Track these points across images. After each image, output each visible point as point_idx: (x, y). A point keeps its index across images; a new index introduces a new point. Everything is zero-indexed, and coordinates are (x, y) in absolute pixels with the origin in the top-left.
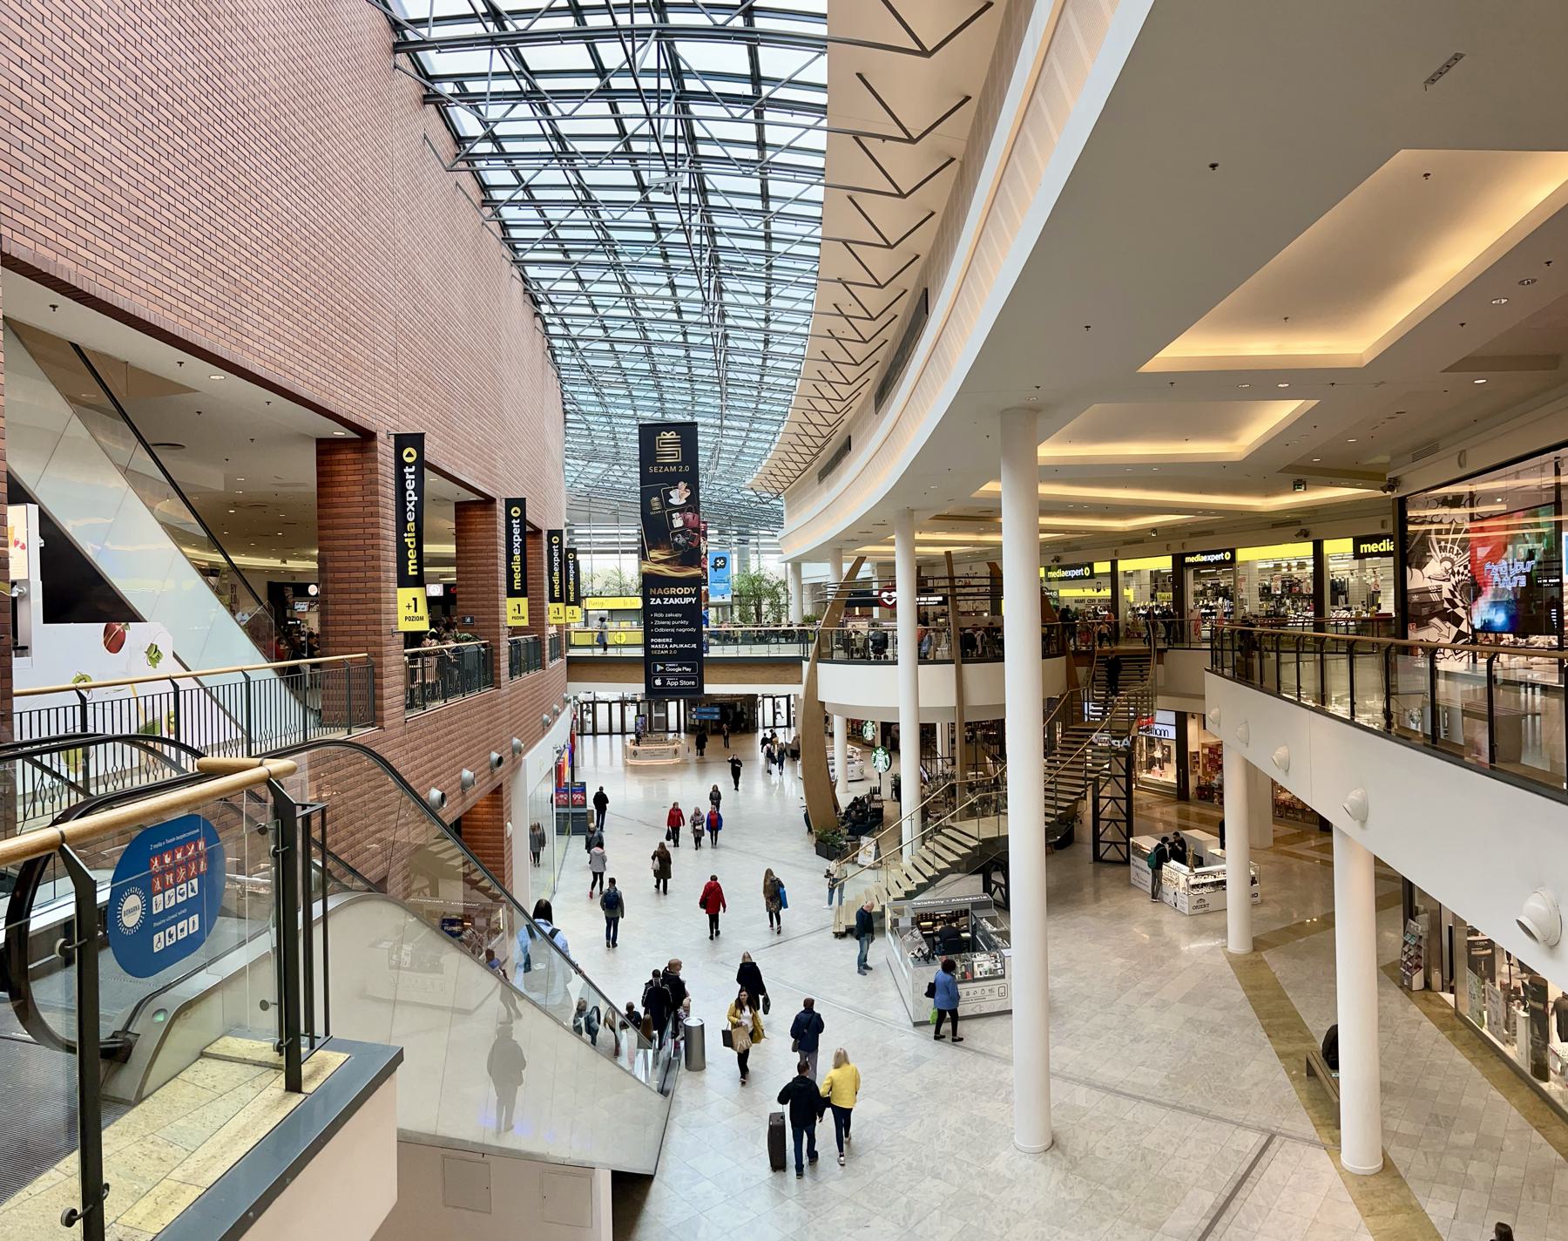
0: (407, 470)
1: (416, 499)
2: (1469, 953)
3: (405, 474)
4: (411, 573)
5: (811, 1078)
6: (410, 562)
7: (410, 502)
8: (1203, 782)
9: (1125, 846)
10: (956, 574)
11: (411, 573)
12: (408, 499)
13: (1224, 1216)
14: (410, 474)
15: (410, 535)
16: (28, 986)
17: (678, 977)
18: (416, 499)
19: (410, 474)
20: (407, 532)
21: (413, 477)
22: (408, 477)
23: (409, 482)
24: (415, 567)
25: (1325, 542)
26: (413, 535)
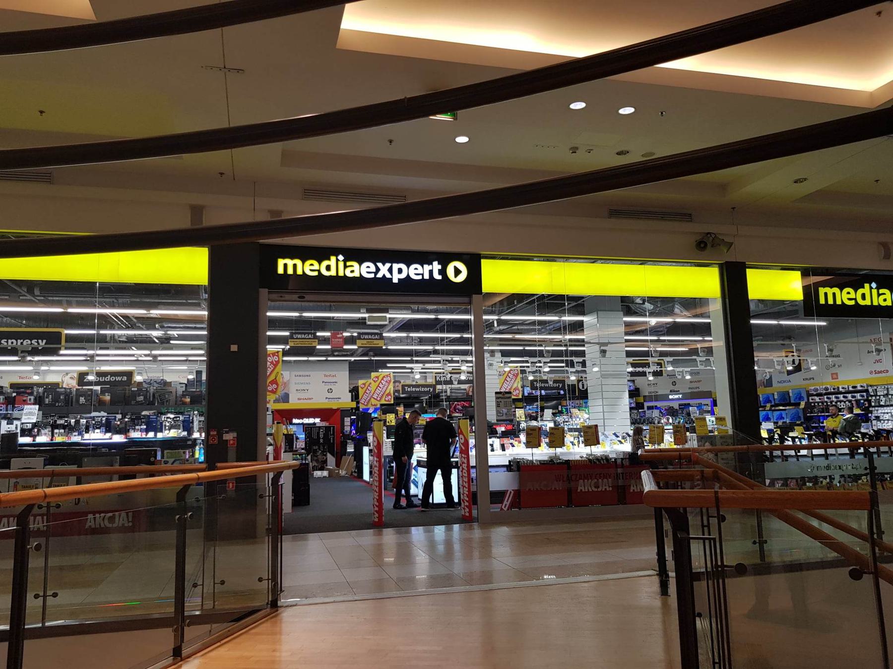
0: (436, 266)
1: (395, 281)
2: (404, 508)
3: (430, 263)
4: (281, 262)
5: (802, 301)
6: (298, 262)
7: (390, 270)
8: (632, 388)
9: (216, 582)
10: (267, 578)
11: (281, 262)
12: (396, 267)
13: (188, 560)
14: (431, 272)
15: (341, 264)
16: (804, 298)
17: (803, 300)
18: (395, 281)
19: (431, 272)
20: (345, 261)
21: (427, 277)
22: (427, 268)
23: (316, 265)
24: (290, 271)
25: (490, 490)
26: (341, 274)
